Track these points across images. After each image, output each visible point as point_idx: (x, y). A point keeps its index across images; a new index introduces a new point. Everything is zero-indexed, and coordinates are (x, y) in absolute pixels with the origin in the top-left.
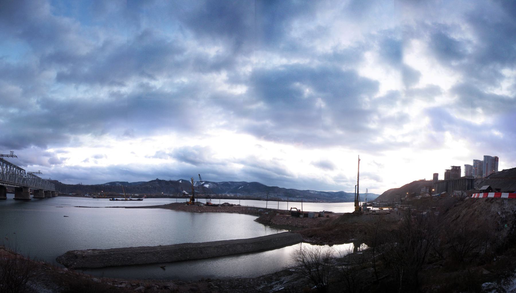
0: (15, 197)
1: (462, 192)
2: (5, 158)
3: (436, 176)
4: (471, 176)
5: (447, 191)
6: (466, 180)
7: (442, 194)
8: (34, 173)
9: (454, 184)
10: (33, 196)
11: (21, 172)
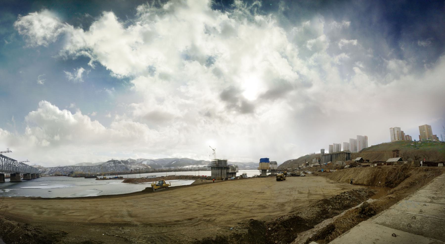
0: (11, 180)
1: (343, 162)
2: (3, 154)
3: (322, 151)
4: (349, 151)
5: (331, 161)
6: (345, 153)
7: (328, 163)
8: (23, 162)
9: (336, 156)
10: (23, 178)
11: (15, 162)
